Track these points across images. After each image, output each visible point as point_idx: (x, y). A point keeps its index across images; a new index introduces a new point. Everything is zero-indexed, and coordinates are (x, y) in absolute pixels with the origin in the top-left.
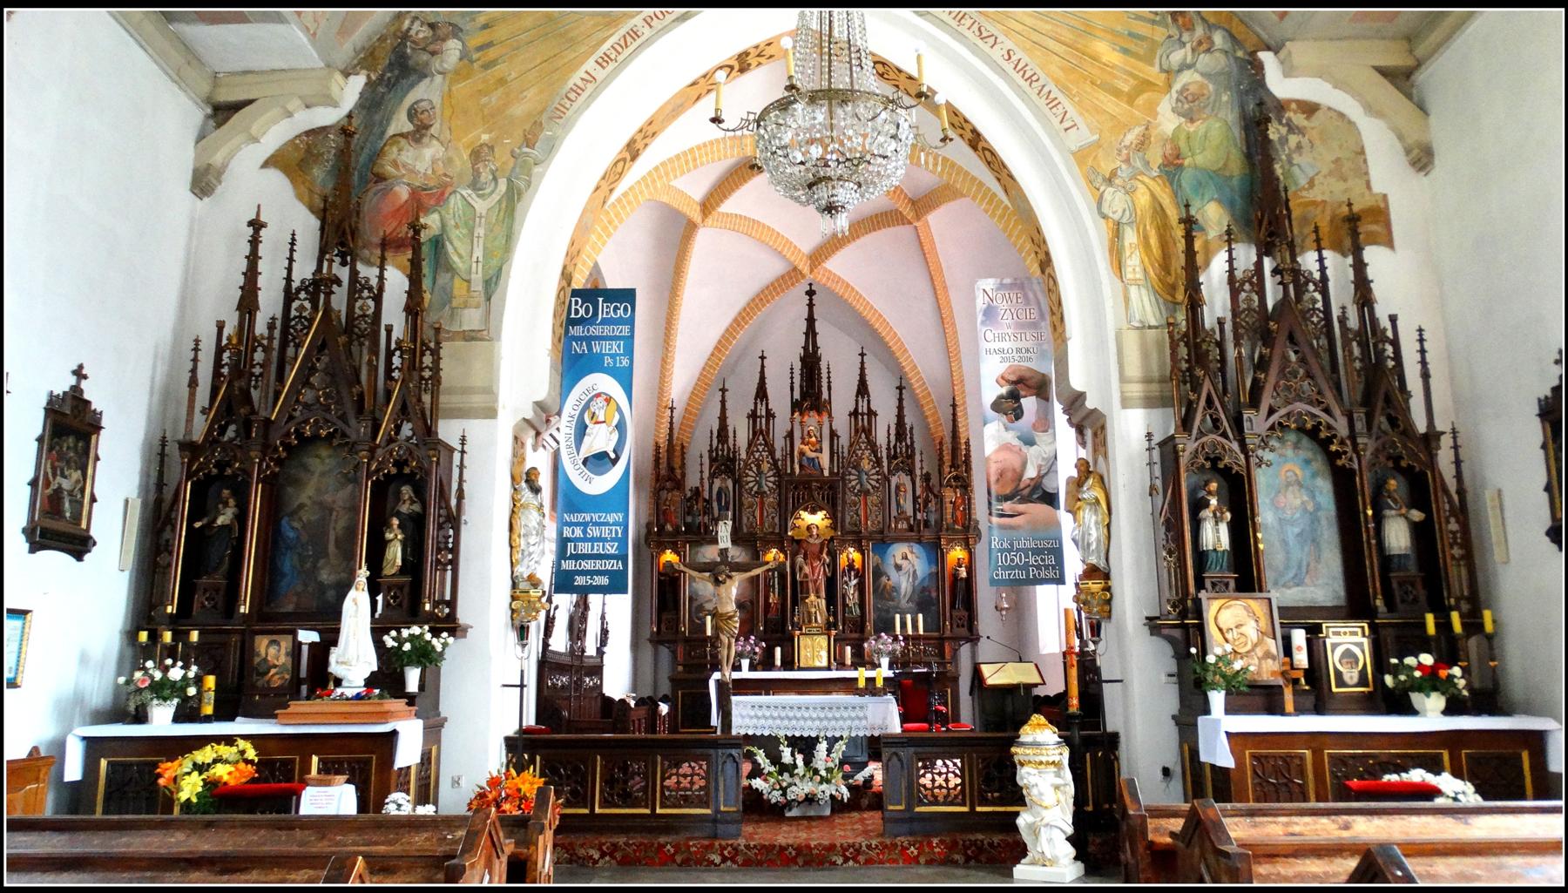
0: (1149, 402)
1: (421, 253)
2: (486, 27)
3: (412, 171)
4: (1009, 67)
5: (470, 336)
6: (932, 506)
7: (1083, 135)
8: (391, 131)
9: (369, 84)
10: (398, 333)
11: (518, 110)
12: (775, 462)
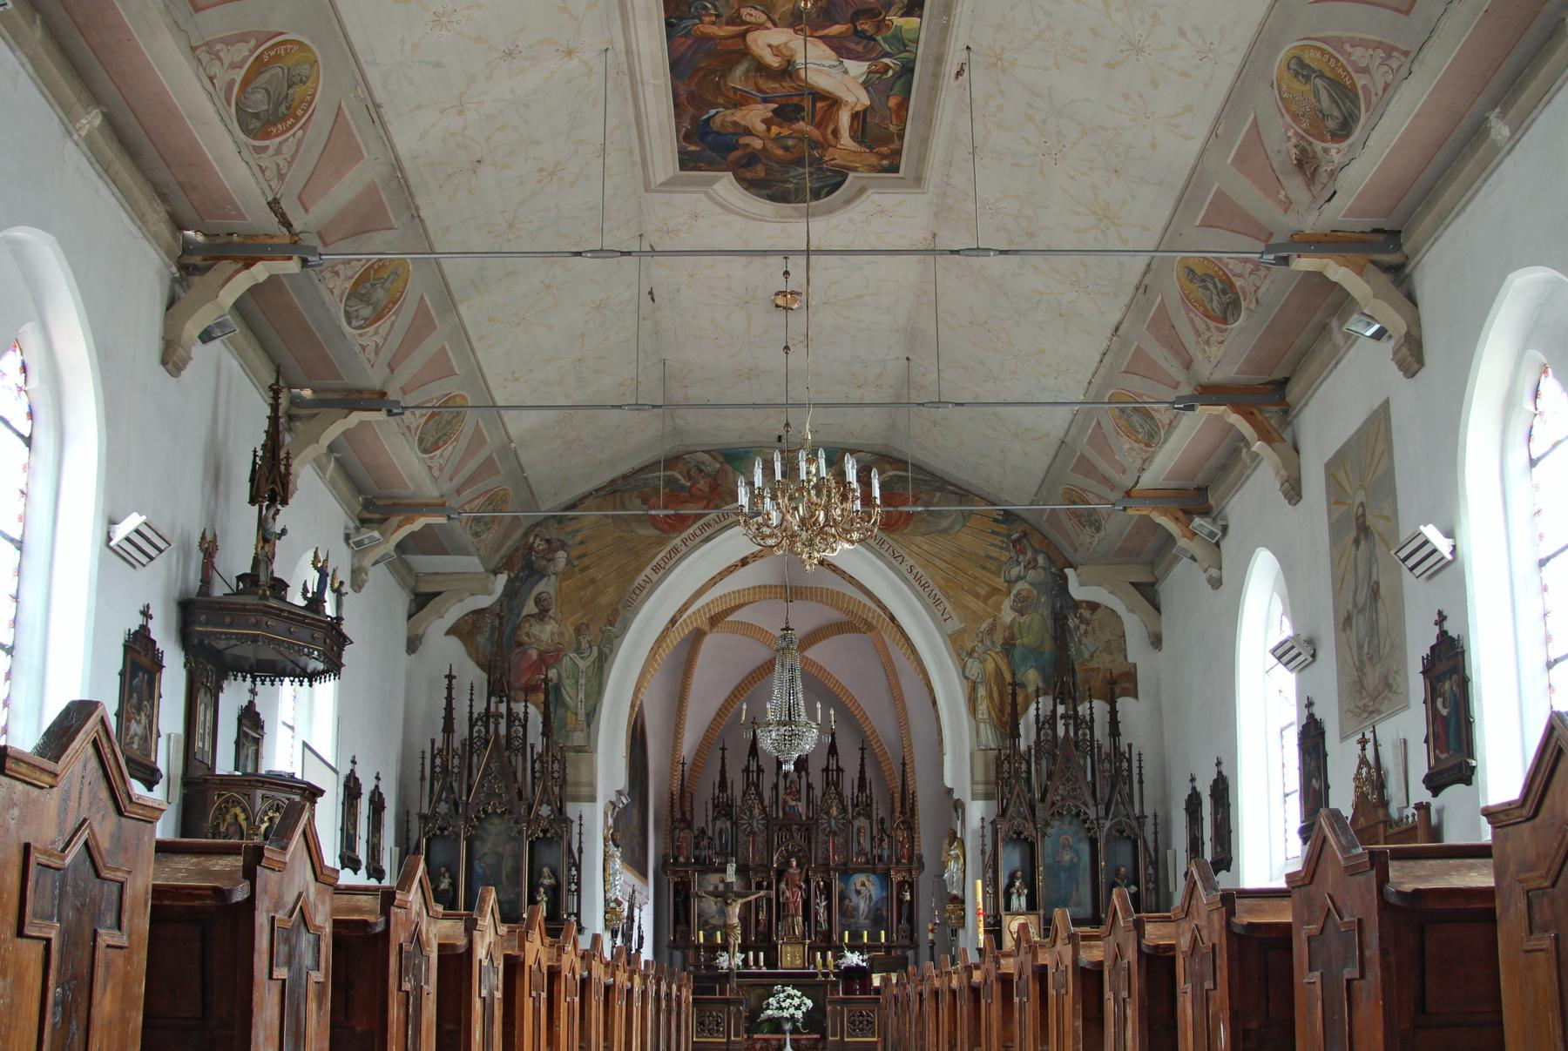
0: (987, 796)
1: (551, 699)
2: (582, 543)
3: (539, 640)
4: (910, 577)
5: (579, 750)
6: (885, 844)
7: (955, 625)
8: (525, 613)
9: (509, 580)
10: (539, 749)
11: (604, 600)
12: (764, 809)
